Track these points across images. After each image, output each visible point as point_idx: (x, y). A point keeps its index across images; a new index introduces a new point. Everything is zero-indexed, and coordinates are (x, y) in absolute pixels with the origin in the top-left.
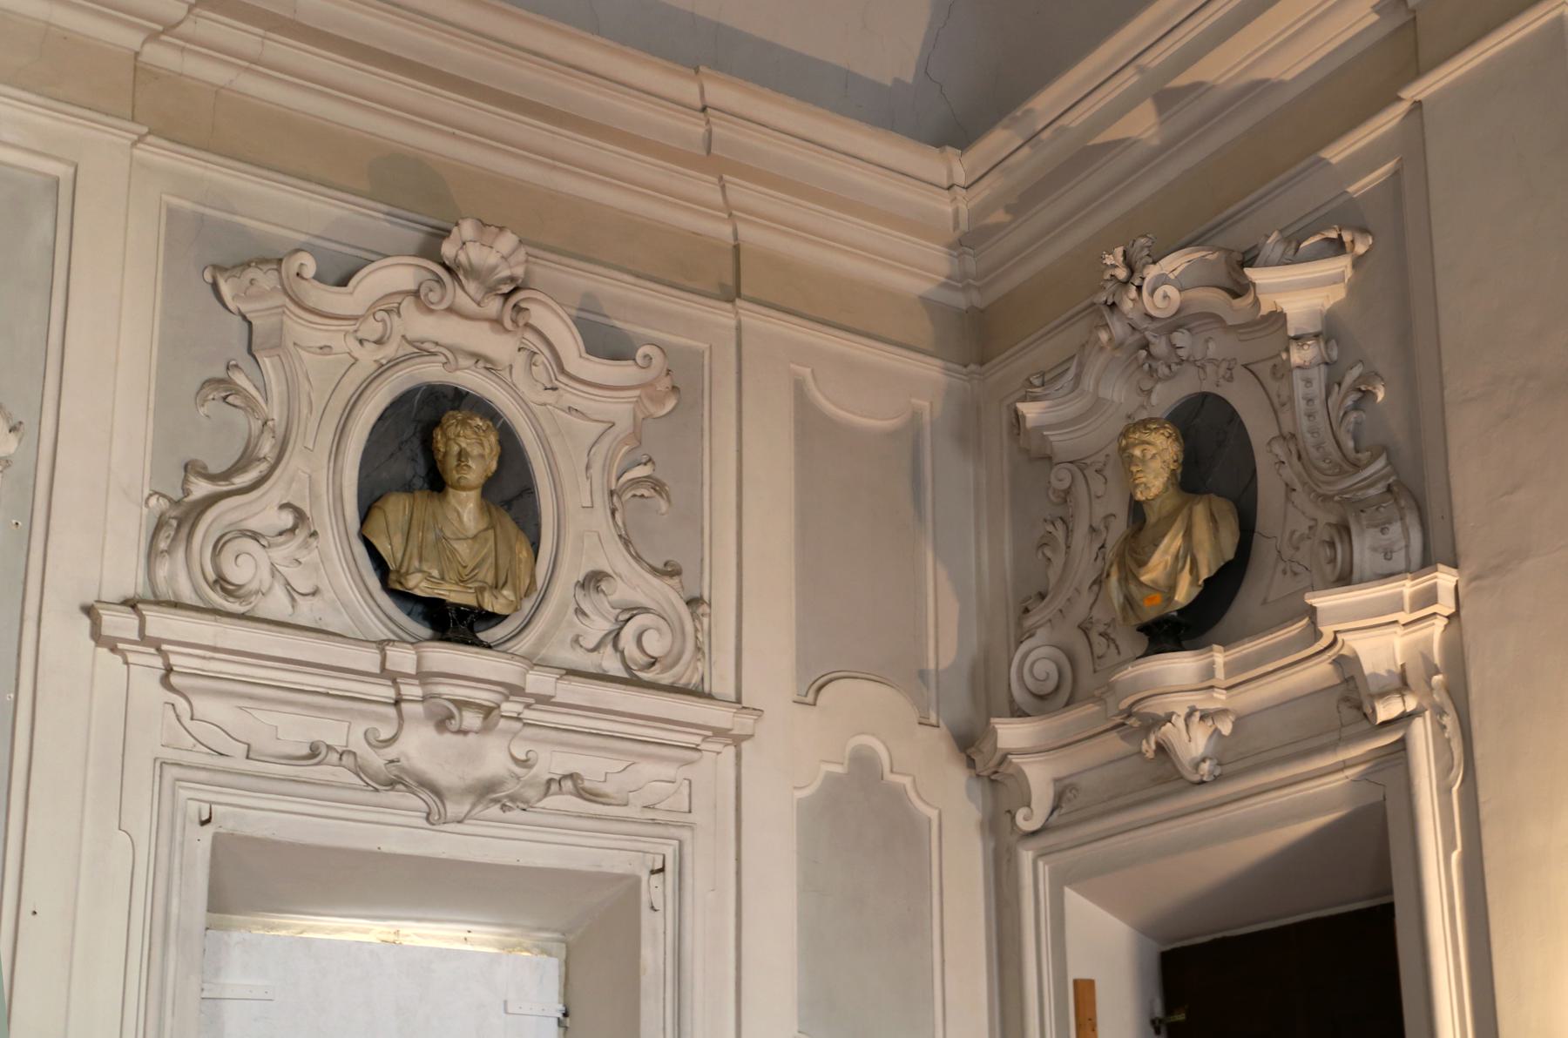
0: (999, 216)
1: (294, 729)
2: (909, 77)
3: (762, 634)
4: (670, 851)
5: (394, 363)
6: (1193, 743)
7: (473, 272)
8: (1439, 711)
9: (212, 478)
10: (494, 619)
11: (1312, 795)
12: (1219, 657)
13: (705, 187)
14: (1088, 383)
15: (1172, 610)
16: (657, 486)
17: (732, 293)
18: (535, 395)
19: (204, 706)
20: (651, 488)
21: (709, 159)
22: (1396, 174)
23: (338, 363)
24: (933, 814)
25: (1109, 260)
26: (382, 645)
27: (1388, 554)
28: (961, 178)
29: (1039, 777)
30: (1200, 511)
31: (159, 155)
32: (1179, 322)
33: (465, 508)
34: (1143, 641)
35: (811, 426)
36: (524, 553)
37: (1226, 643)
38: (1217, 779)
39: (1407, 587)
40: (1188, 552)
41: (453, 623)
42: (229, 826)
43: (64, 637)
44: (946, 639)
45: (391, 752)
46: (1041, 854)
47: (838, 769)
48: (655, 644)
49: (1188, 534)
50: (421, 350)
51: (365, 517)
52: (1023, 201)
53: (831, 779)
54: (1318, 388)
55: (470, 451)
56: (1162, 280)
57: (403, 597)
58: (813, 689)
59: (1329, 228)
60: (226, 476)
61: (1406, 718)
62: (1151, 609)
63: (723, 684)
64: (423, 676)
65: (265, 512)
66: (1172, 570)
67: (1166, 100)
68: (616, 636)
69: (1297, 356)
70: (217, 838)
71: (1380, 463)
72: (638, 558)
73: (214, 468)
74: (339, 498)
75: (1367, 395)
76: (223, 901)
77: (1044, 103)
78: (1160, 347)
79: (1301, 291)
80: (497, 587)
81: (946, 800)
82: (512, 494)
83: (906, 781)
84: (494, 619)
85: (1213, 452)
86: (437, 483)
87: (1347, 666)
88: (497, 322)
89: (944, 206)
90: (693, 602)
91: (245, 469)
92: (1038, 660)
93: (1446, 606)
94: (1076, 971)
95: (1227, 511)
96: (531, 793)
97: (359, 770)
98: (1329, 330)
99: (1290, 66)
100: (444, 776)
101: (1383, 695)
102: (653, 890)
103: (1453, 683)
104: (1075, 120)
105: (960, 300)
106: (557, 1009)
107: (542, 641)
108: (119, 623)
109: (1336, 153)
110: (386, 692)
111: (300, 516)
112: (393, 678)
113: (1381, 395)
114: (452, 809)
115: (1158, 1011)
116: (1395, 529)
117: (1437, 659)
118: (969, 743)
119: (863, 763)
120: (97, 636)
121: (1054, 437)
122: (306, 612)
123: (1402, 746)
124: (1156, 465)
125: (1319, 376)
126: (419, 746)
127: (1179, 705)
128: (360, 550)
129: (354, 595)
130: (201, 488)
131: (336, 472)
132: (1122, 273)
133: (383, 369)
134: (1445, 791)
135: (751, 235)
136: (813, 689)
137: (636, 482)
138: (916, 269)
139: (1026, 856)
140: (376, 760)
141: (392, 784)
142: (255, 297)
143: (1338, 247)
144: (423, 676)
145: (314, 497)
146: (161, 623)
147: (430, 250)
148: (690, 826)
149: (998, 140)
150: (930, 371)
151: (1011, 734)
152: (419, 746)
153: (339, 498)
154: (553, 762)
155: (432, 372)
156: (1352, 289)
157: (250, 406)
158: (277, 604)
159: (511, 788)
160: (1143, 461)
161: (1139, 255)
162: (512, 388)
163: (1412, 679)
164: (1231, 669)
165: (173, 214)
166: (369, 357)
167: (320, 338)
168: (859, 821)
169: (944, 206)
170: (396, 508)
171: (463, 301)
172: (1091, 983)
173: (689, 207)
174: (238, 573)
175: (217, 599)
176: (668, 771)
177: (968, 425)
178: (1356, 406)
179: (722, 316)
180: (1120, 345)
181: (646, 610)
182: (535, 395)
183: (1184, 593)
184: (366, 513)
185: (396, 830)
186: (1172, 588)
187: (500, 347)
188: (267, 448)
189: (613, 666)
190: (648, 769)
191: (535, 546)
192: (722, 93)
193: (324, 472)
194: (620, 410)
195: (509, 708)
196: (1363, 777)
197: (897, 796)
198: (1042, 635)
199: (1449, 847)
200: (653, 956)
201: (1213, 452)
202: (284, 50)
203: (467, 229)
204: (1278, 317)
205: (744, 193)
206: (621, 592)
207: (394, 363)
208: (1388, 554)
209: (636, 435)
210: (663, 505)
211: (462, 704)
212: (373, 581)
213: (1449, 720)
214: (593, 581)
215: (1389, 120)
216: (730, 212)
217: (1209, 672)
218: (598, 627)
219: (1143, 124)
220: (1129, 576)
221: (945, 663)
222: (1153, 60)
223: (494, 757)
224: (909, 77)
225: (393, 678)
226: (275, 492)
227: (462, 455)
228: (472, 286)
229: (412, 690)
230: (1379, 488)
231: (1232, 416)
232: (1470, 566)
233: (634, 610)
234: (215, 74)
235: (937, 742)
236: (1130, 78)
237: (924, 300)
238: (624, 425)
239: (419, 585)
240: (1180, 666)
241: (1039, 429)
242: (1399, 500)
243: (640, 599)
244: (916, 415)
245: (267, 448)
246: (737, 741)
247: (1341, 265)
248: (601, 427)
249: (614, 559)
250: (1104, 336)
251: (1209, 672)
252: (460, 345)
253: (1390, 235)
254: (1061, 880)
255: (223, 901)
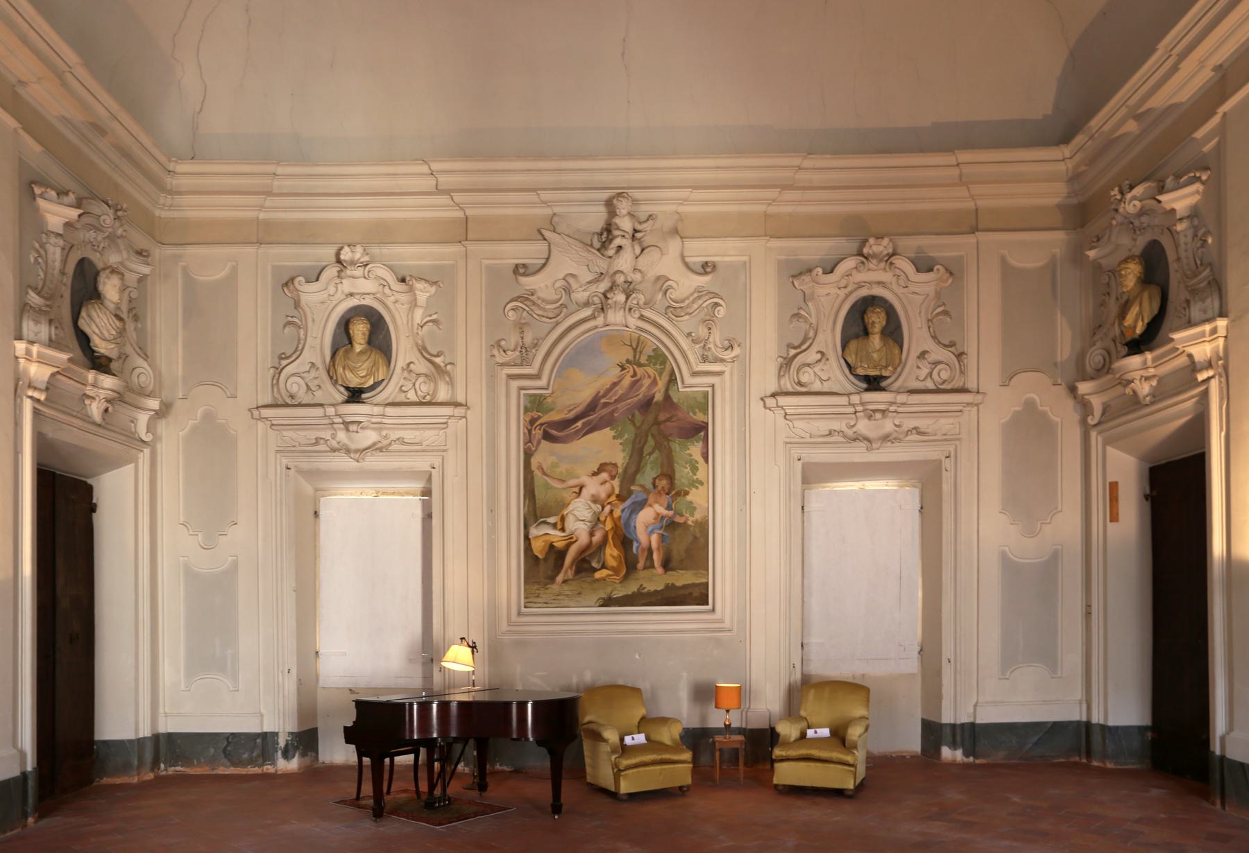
0: (1083, 168)
1: (823, 426)
2: (1050, 112)
3: (986, 364)
4: (952, 449)
5: (851, 293)
6: (1144, 389)
7: (874, 256)
8: (1220, 376)
9: (795, 348)
10: (886, 378)
11: (1181, 408)
12: (1149, 356)
13: (962, 192)
14: (1113, 239)
15: (1136, 336)
16: (945, 313)
17: (974, 230)
18: (900, 291)
19: (797, 423)
20: (945, 312)
21: (962, 181)
22: (1219, 142)
23: (831, 298)
24: (1058, 420)
25: (1113, 193)
26: (848, 395)
27: (1205, 312)
28: (1067, 154)
29: (1097, 403)
30: (1146, 295)
31: (775, 243)
32: (1142, 213)
33: (876, 340)
34: (1125, 350)
35: (1008, 273)
36: (897, 351)
37: (1151, 350)
38: (1152, 403)
39: (1207, 327)
40: (1140, 314)
41: (873, 383)
42: (806, 460)
43: (756, 407)
44: (1065, 345)
45: (855, 429)
46: (1099, 433)
47: (1018, 409)
48: (944, 375)
49: (1141, 305)
50: (860, 286)
51: (843, 349)
52: (1092, 161)
53: (1016, 412)
54: (1189, 239)
55: (877, 320)
56: (1134, 198)
57: (856, 376)
58: (1007, 379)
59: (1190, 172)
60: (799, 346)
61: (1209, 379)
62: (1129, 338)
63: (971, 385)
64: (862, 404)
65: (812, 356)
66: (1136, 322)
67: (1137, 118)
68: (931, 374)
69: (1180, 227)
70: (803, 465)
71: (1207, 272)
72: (939, 343)
73: (796, 344)
74: (835, 345)
75: (1205, 241)
76: (807, 480)
77: (1095, 123)
78: (1137, 223)
79: (1181, 200)
80: (886, 367)
81: (1064, 415)
82: (893, 332)
83: (1047, 409)
84: (886, 378)
85: (1154, 264)
86: (866, 333)
87: (1190, 356)
88: (884, 269)
89: (1062, 167)
90: (959, 356)
91: (801, 347)
92: (1095, 357)
93: (1222, 332)
94: (1110, 479)
95: (1155, 292)
96: (901, 436)
97: (845, 436)
98: (1194, 214)
99: (1184, 96)
100: (871, 435)
101: (1201, 370)
102: (947, 464)
103: (1223, 364)
104: (1106, 128)
105: (1074, 201)
106: (918, 506)
107: (905, 381)
108: (771, 402)
109: (1199, 134)
110: (852, 410)
111: (822, 353)
112: (854, 405)
113: (1210, 241)
114: (874, 446)
115: (1148, 491)
116: (1209, 301)
117: (1221, 354)
118: (1073, 390)
119: (1030, 406)
120: (765, 407)
121: (1103, 262)
122: (826, 387)
123: (1206, 394)
124: (1131, 277)
125: (1190, 233)
126: (863, 426)
127: (1137, 375)
128: (842, 362)
129: (841, 378)
130: (793, 352)
131: (834, 337)
132: (1119, 197)
133: (847, 296)
134: (1221, 408)
135: (981, 203)
136: (1007, 379)
137: (938, 314)
138: (1053, 194)
139: (1093, 434)
140: (850, 432)
141: (855, 440)
142: (805, 284)
143: (1198, 179)
144: (862, 404)
145: (827, 346)
146: (782, 400)
147: (860, 254)
148: (959, 439)
149: (1079, 139)
150: (1060, 236)
151: (1084, 388)
152: (863, 426)
153: (835, 345)
154: (909, 423)
155: (864, 292)
156: (1205, 193)
157: (806, 320)
158: (817, 386)
159: (895, 435)
160: (1126, 276)
161: (1125, 188)
162: (891, 290)
163: (1213, 363)
164: (1154, 360)
165: (779, 262)
166: (842, 293)
167: (825, 291)
168: (1029, 429)
169: (1062, 167)
170: (853, 345)
171: (871, 266)
172: (1116, 483)
173: (955, 200)
174: (804, 379)
175: (799, 389)
176: (951, 420)
177: (1076, 256)
178: (1202, 246)
179: (971, 239)
180: (1122, 224)
181: (940, 362)
182: (900, 291)
183: (1139, 329)
184: (844, 347)
185: (858, 454)
186: (1135, 327)
187: (887, 277)
188: (811, 334)
189: (931, 385)
190: (943, 421)
191: (901, 348)
192: (964, 156)
193: (830, 337)
194: (930, 289)
195: (892, 408)
196: (1197, 403)
197: (1044, 415)
198: (1099, 344)
199: (1221, 430)
200: (947, 487)
201: (1154, 264)
202: (810, 195)
203: (872, 241)
204: (1173, 211)
205: (977, 189)
206: (932, 357)
207: (851, 293)
208: (1205, 312)
209: (938, 295)
210: (948, 320)
211: (874, 411)
212: (847, 371)
213: (1223, 380)
214: (923, 355)
215: (1215, 121)
216: (972, 197)
217: (1145, 362)
218: (925, 371)
219: (1132, 127)
220: (1121, 324)
221: (1065, 357)
222: (1132, 102)
223: (888, 426)
224: (1050, 112)
225: (854, 405)
226: (815, 348)
227: (873, 323)
228: (874, 261)
229: (860, 408)
230: (1205, 283)
231: (1163, 250)
232: (1232, 315)
233: (936, 363)
234: (789, 209)
235: (1062, 391)
236: (1124, 111)
237: (1059, 206)
238: (932, 294)
239: (861, 372)
240: (1135, 360)
241: (1095, 260)
242: (1213, 289)
243: (939, 358)
244: (1054, 256)
245: (811, 334)
246: (977, 405)
247: (1197, 186)
248: (922, 298)
249: (930, 345)
250: (1114, 222)
251: (1145, 362)
252: (875, 280)
253: (1209, 167)
254: (1106, 442)
255: (807, 480)
